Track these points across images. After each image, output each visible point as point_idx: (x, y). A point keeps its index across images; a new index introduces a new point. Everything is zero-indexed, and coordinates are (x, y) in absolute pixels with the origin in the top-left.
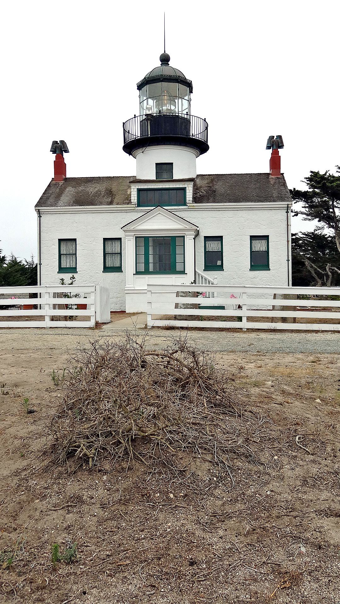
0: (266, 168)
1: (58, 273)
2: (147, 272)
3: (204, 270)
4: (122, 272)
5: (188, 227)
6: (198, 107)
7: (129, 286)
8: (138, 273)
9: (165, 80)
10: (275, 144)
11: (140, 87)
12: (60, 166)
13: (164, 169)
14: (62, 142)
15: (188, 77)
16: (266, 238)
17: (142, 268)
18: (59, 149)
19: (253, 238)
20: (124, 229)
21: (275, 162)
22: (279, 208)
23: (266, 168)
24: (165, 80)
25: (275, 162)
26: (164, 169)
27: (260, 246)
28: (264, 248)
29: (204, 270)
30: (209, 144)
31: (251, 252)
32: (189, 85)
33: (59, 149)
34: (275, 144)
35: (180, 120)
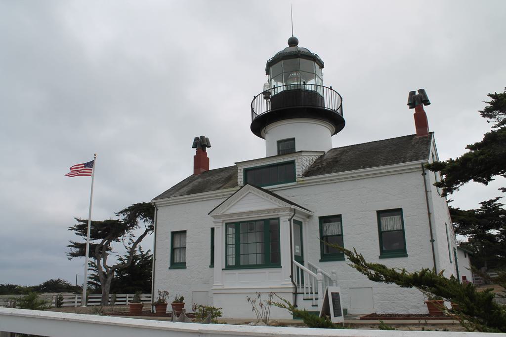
0: (412, 130)
1: (170, 268)
2: (238, 266)
3: (321, 261)
4: (407, 256)
5: (281, 206)
6: (333, 83)
7: (217, 284)
8: (228, 267)
9: (294, 60)
10: (418, 101)
11: (268, 73)
12: (201, 160)
13: (287, 146)
14: (202, 137)
15: (313, 51)
16: (398, 211)
17: (232, 262)
18: (201, 144)
19: (381, 214)
20: (212, 214)
21: (421, 120)
22: (411, 171)
23: (412, 130)
24: (294, 60)
25: (421, 120)
26: (287, 146)
27: (391, 224)
28: (398, 227)
29: (321, 261)
30: (344, 117)
31: (381, 233)
32: (314, 58)
33: (201, 144)
34: (418, 101)
35: (303, 93)
